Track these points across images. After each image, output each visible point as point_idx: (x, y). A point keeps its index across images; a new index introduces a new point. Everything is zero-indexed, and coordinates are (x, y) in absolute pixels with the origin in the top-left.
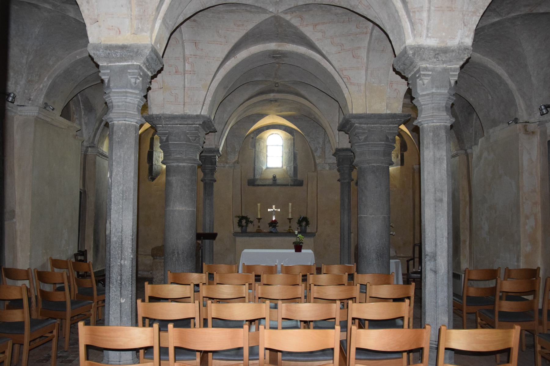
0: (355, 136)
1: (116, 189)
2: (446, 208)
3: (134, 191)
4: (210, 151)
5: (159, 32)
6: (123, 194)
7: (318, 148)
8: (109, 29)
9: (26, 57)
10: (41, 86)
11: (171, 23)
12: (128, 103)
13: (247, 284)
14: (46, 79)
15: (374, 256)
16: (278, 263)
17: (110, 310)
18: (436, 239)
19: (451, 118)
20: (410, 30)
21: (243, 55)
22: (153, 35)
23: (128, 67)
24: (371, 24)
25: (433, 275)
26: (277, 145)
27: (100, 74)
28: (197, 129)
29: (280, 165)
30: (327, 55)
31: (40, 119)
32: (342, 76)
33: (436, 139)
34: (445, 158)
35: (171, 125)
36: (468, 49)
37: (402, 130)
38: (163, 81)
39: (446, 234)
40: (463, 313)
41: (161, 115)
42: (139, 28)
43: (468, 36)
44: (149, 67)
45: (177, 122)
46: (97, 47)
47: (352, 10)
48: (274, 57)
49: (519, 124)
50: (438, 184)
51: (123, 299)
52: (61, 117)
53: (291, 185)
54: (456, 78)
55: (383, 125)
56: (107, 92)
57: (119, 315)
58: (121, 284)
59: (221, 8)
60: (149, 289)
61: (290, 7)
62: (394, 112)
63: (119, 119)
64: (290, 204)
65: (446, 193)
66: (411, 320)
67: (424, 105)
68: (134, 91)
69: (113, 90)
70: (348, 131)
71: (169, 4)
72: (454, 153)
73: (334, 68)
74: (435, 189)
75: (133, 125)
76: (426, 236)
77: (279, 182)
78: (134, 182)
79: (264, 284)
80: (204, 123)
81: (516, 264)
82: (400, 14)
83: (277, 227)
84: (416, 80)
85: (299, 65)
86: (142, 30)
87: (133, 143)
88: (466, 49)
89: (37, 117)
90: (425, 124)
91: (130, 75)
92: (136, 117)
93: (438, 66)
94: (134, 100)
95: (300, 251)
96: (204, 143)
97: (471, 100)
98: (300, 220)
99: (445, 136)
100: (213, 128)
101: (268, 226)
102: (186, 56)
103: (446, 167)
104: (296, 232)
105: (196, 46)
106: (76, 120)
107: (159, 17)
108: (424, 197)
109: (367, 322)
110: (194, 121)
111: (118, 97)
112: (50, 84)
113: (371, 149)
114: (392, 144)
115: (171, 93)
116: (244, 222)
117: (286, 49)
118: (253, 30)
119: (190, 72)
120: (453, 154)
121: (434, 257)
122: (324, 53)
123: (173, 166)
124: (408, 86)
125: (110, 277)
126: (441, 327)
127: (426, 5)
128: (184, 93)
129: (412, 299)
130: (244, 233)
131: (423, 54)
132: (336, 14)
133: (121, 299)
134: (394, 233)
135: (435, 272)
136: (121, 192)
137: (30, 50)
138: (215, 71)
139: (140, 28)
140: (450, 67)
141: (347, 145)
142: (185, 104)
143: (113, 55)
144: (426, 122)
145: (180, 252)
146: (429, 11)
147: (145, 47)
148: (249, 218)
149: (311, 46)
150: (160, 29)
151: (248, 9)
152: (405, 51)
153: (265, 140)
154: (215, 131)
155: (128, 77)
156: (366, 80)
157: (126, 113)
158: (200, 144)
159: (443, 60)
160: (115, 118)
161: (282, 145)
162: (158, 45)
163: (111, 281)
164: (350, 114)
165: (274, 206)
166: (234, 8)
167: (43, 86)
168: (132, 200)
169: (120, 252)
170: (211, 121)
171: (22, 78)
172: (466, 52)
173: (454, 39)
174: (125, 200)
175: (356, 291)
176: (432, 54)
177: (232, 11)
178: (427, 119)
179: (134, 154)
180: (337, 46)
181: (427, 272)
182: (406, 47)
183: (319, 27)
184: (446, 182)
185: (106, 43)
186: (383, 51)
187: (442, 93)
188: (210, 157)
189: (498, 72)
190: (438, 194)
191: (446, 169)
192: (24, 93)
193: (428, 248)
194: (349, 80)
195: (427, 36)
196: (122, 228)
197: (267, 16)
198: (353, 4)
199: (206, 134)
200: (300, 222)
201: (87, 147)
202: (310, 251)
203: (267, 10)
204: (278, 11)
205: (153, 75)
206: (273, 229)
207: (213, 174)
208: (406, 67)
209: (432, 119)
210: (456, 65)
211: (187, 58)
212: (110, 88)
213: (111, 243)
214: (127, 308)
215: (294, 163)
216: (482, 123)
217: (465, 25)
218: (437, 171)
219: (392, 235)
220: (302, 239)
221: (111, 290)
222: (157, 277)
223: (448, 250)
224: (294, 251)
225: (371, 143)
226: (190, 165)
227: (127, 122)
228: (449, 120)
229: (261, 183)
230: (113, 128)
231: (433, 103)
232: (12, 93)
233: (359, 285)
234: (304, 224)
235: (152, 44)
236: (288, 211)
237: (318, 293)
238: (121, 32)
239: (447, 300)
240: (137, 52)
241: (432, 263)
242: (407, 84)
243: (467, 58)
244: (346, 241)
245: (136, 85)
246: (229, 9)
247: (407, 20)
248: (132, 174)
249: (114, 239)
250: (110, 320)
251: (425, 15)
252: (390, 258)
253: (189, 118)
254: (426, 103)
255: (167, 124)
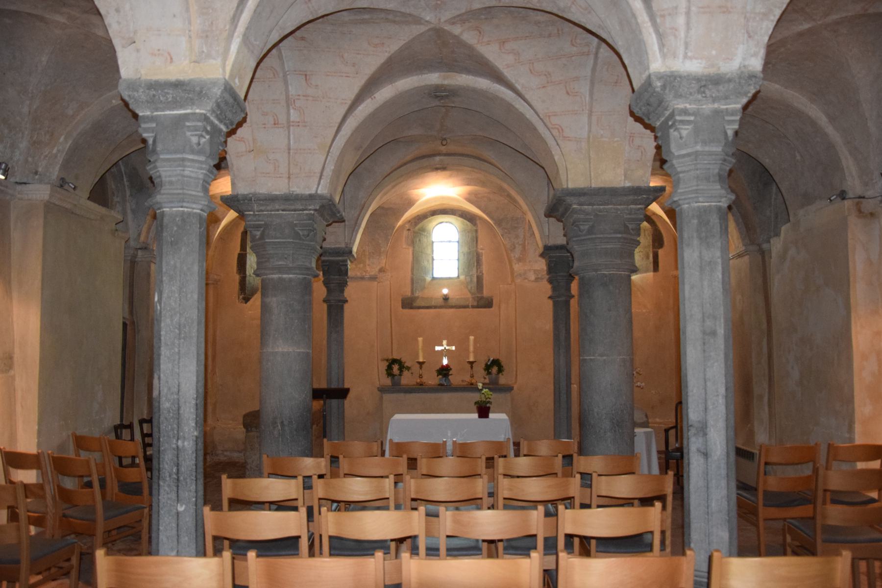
0: (572, 225)
1: (168, 321)
2: (722, 347)
3: (199, 324)
4: (337, 252)
5: (236, 58)
6: (179, 329)
7: (517, 246)
8: (153, 54)
9: (28, 102)
10: (55, 151)
11: (258, 43)
12: (187, 177)
13: (392, 477)
14: (62, 139)
15: (607, 424)
16: (450, 439)
17: (160, 524)
18: (706, 398)
19: (728, 194)
20: (656, 47)
21: (385, 93)
22: (227, 63)
23: (186, 117)
24: (596, 40)
25: (702, 460)
26: (450, 242)
27: (140, 130)
28: (311, 217)
29: (454, 273)
30: (523, 92)
31: (54, 204)
32: (550, 126)
33: (703, 229)
34: (719, 260)
35: (268, 211)
36: (755, 77)
37: (654, 214)
38: (254, 140)
39: (722, 390)
40: (757, 520)
41: (251, 195)
42: (203, 52)
43: (755, 55)
44: (221, 117)
45: (277, 207)
46: (133, 85)
47: (560, 15)
48: (437, 97)
49: (849, 200)
50: (708, 305)
51: (181, 506)
52: (88, 201)
53: (473, 307)
54: (736, 127)
55: (619, 207)
56: (152, 160)
57: (174, 532)
58: (178, 480)
59: (346, 16)
60: (228, 487)
61: (458, 13)
62: (637, 184)
63: (172, 205)
64: (472, 338)
65: (722, 320)
66: (668, 534)
67: (684, 172)
68: (196, 157)
69: (162, 157)
70: (563, 215)
71: (253, 11)
72: (741, 250)
73: (536, 113)
74: (703, 313)
75: (196, 213)
76: (690, 394)
77: (451, 302)
78: (198, 309)
79: (423, 475)
80: (322, 206)
81: (847, 435)
82: (639, 21)
83: (450, 377)
84: (669, 132)
85: (478, 110)
86: (209, 56)
87: (197, 244)
88: (752, 76)
89: (48, 202)
90: (684, 204)
91: (189, 131)
92: (202, 201)
93: (704, 107)
94: (196, 172)
95: (487, 416)
96: (324, 240)
97: (766, 162)
98: (489, 363)
99: (719, 225)
100: (338, 215)
101: (436, 374)
102: (290, 97)
103: (720, 276)
104: (480, 386)
105: (306, 80)
106: (118, 206)
107: (236, 34)
108: (685, 327)
109: (593, 542)
110: (306, 205)
111: (170, 167)
112: (70, 147)
113: (599, 247)
114: (634, 237)
115: (268, 158)
116: (396, 368)
117: (457, 83)
118: (401, 50)
119: (297, 124)
120: (738, 252)
121: (703, 429)
122: (519, 87)
123: (272, 279)
124: (655, 141)
125: (159, 468)
126: (712, 554)
127: (683, 5)
128: (289, 158)
129: (670, 499)
130: (396, 387)
131: (679, 87)
132: (537, 23)
133: (179, 504)
134: (643, 384)
135: (706, 455)
136: (177, 326)
137: (34, 91)
138: (339, 120)
139: (205, 51)
140: (725, 107)
141: (561, 240)
142: (291, 176)
143: (162, 98)
144: (686, 201)
145: (286, 423)
146: (688, 13)
147: (214, 83)
148: (405, 362)
149: (499, 78)
150: (238, 53)
151: (391, 17)
152: (648, 83)
153: (429, 234)
154: (342, 221)
155: (185, 133)
156: (590, 131)
157: (184, 194)
158: (316, 242)
159: (714, 95)
160: (165, 202)
161: (457, 240)
162: (237, 81)
163: (161, 476)
164: (563, 190)
165: (445, 342)
166: (366, 16)
167: (59, 151)
168: (195, 340)
169: (175, 426)
170: (334, 205)
171: (22, 137)
172: (752, 82)
173: (731, 59)
174: (184, 339)
175: (574, 487)
176: (695, 86)
177: (364, 22)
178: (686, 197)
179: (199, 263)
180: (540, 75)
181: (691, 454)
182: (649, 76)
183: (508, 46)
184: (721, 302)
185: (149, 78)
186: (616, 83)
187: (713, 151)
188: (337, 263)
189: (810, 114)
190: (709, 323)
191: (721, 281)
192: (26, 161)
193: (693, 414)
194: (561, 131)
195: (686, 57)
196: (179, 386)
197: (423, 29)
198: (562, 5)
199: (327, 226)
200: (488, 368)
201: (137, 249)
202: (504, 416)
203: (421, 18)
204: (440, 19)
205: (229, 130)
206: (444, 379)
207: (342, 291)
208: (651, 109)
209: (696, 195)
210: (735, 103)
211: (292, 100)
212: (157, 154)
213: (161, 412)
214: (188, 521)
215: (477, 269)
216: (785, 198)
217: (750, 37)
218: (706, 283)
219: (640, 387)
220: (490, 396)
221: (162, 491)
222: (253, 462)
223: (727, 417)
224: (476, 416)
225: (599, 236)
226: (301, 276)
227: (186, 210)
228: (726, 197)
229: (423, 304)
230: (162, 219)
231: (697, 170)
232: (3, 163)
233: (578, 476)
234: (495, 370)
235: (225, 79)
236: (467, 350)
237: (510, 490)
238: (174, 59)
239: (726, 503)
240: (201, 92)
241: (701, 440)
242: (653, 137)
243: (753, 91)
244: (564, 397)
245: (200, 147)
246: (359, 18)
247: (651, 30)
248: (196, 296)
249: (165, 405)
250: (160, 540)
251: (681, 20)
252: (635, 425)
253: (297, 200)
254: (687, 169)
255: (262, 211)
